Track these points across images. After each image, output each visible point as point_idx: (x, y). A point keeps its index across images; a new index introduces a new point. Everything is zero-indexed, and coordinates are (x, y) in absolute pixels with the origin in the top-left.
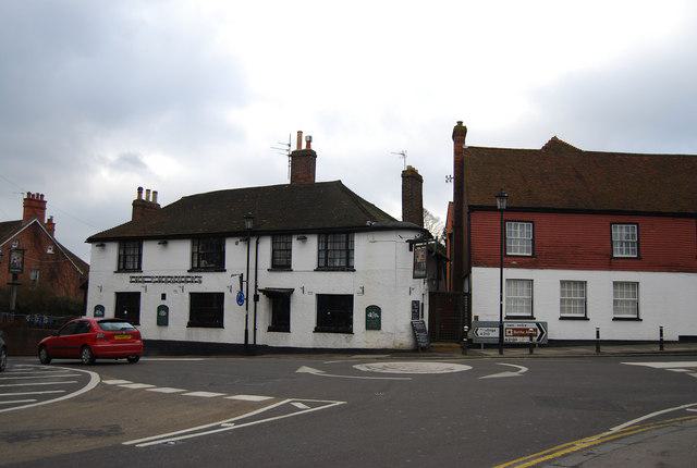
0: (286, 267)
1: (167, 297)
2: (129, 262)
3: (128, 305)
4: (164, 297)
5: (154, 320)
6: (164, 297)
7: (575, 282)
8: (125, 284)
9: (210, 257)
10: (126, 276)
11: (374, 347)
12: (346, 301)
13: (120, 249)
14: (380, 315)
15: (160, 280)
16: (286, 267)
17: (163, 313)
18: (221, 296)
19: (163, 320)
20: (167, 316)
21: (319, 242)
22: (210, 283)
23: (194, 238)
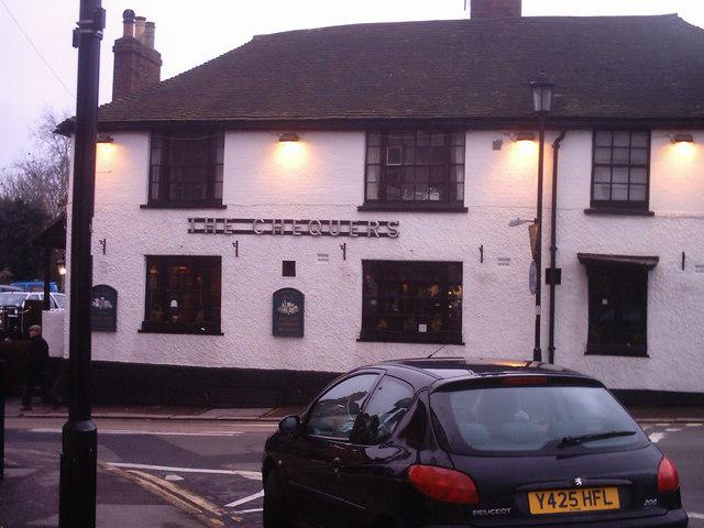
0: (638, 208)
1: (299, 269)
2: (186, 177)
3: (186, 293)
4: (289, 268)
5: (264, 321)
6: (289, 268)
7: (540, 231)
8: (174, 234)
9: (417, 170)
10: (178, 219)
11: (556, 326)
12: (206, 271)
13: (152, 149)
14: (115, 303)
15: (278, 228)
16: (638, 208)
17: (289, 308)
18: (370, 267)
19: (288, 317)
20: (300, 316)
21: (368, 147)
22: (420, 238)
23: (381, 133)
